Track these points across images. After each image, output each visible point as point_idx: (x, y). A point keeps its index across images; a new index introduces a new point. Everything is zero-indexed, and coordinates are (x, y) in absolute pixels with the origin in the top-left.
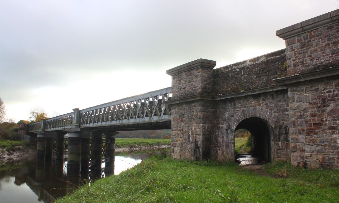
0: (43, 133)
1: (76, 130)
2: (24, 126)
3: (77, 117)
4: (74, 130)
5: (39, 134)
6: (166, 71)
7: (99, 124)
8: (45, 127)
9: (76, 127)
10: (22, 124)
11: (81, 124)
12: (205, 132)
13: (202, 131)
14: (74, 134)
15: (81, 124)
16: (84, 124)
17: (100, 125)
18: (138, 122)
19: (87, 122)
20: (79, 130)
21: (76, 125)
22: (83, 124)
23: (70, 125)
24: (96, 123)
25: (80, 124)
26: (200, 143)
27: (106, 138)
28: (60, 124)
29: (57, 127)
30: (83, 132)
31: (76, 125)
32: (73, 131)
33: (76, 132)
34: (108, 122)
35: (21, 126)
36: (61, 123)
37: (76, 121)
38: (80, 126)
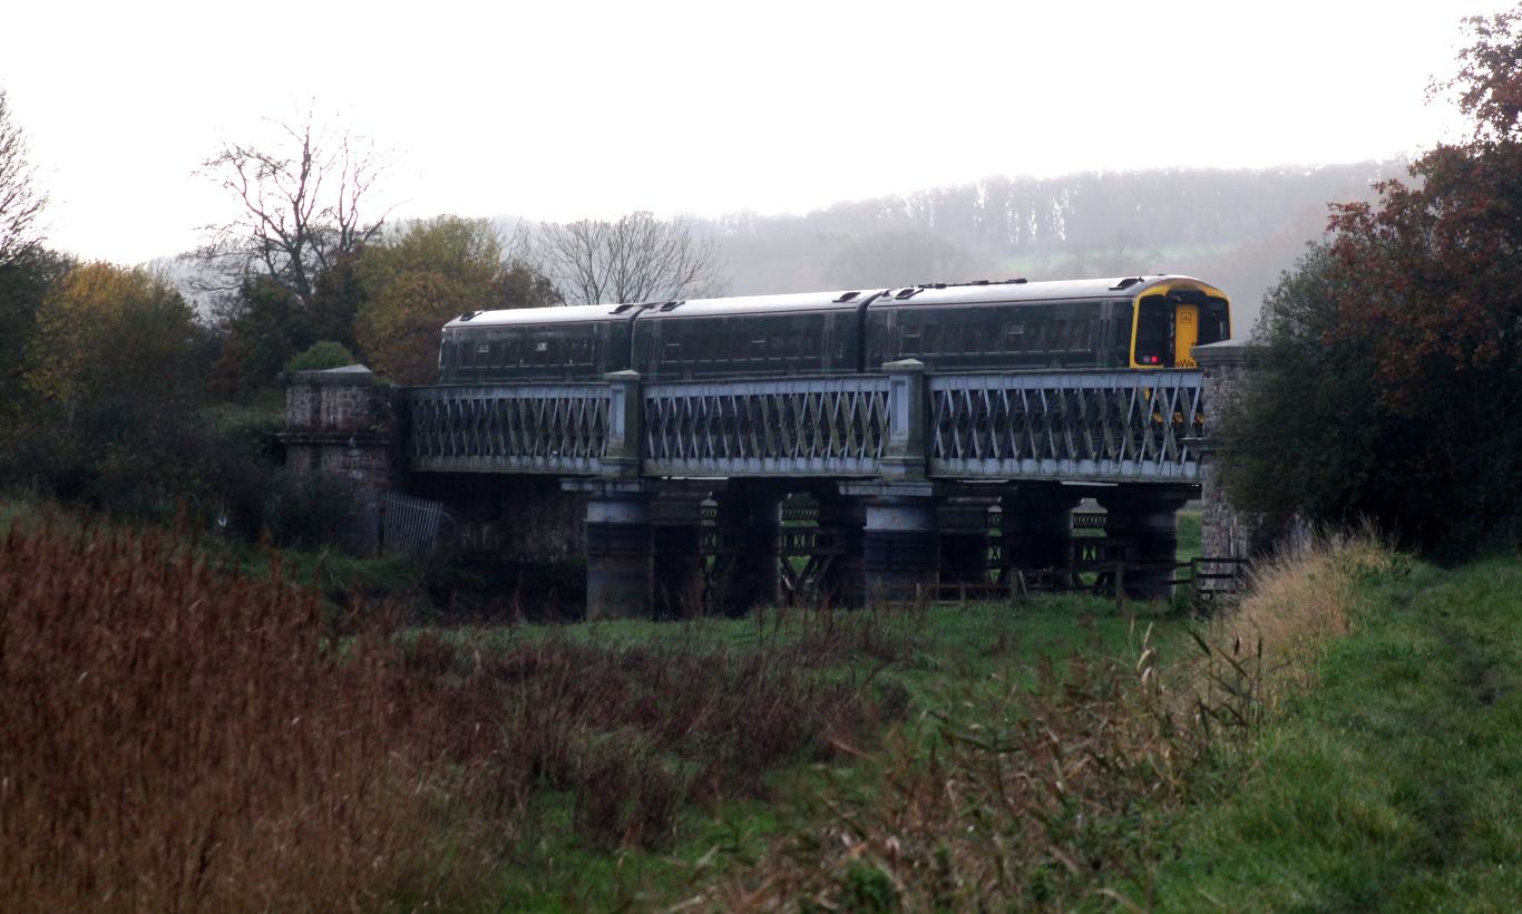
0: (635, 488)
1: (910, 492)
2: (375, 407)
3: (912, 418)
4: (902, 492)
5: (604, 499)
6: (1224, 303)
7: (1029, 467)
8: (643, 440)
9: (906, 473)
10: (354, 390)
11: (649, 453)
12: (1256, 532)
13: (1249, 531)
14: (897, 513)
15: (649, 456)
16: (955, 456)
17: (742, 471)
18: (1167, 478)
19: (986, 446)
20: (928, 492)
21: (906, 463)
22: (946, 458)
23: (849, 455)
24: (1015, 462)
25: (643, 452)
26: (1256, 580)
27: (1106, 530)
28: (785, 434)
29: (750, 454)
30: (950, 499)
31: (906, 463)
32: (894, 500)
33: (908, 504)
34: (1066, 461)
35: (347, 405)
36: (801, 433)
37: (905, 437)
38: (928, 468)
